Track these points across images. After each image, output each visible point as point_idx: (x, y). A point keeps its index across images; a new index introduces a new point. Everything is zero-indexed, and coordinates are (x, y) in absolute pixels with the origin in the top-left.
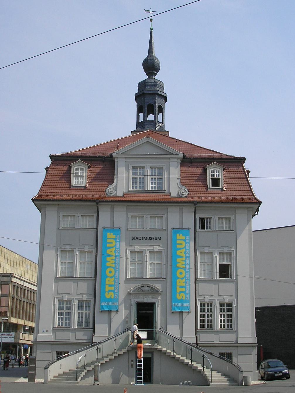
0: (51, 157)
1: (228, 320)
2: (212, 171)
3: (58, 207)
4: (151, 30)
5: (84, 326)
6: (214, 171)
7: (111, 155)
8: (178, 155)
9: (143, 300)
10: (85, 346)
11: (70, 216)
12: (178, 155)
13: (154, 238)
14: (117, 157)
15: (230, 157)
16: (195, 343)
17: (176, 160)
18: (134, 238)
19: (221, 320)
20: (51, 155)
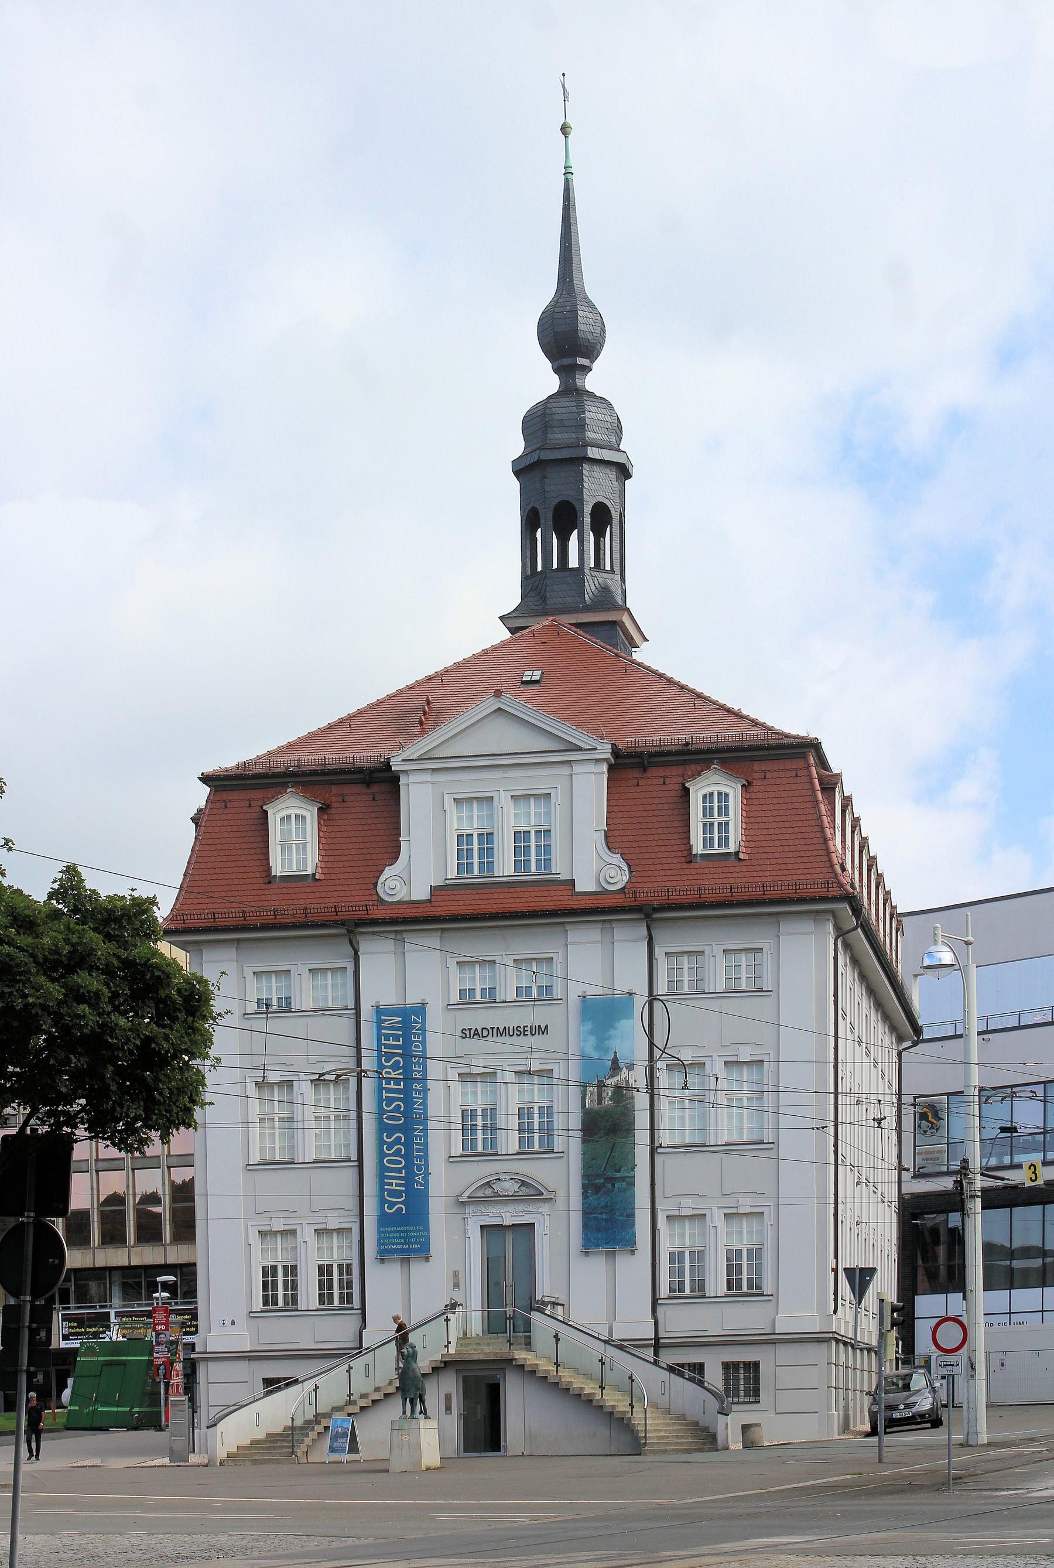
0: (205, 779)
1: (285, 1283)
2: (705, 797)
3: (236, 948)
4: (568, 173)
5: (687, 1291)
6: (711, 794)
7: (387, 765)
8: (596, 749)
9: (499, 1219)
10: (335, 1359)
11: (333, 970)
12: (596, 749)
13: (528, 1028)
14: (406, 772)
15: (785, 741)
16: (650, 1337)
17: (592, 768)
18: (467, 1033)
19: (265, 1285)
20: (202, 774)
